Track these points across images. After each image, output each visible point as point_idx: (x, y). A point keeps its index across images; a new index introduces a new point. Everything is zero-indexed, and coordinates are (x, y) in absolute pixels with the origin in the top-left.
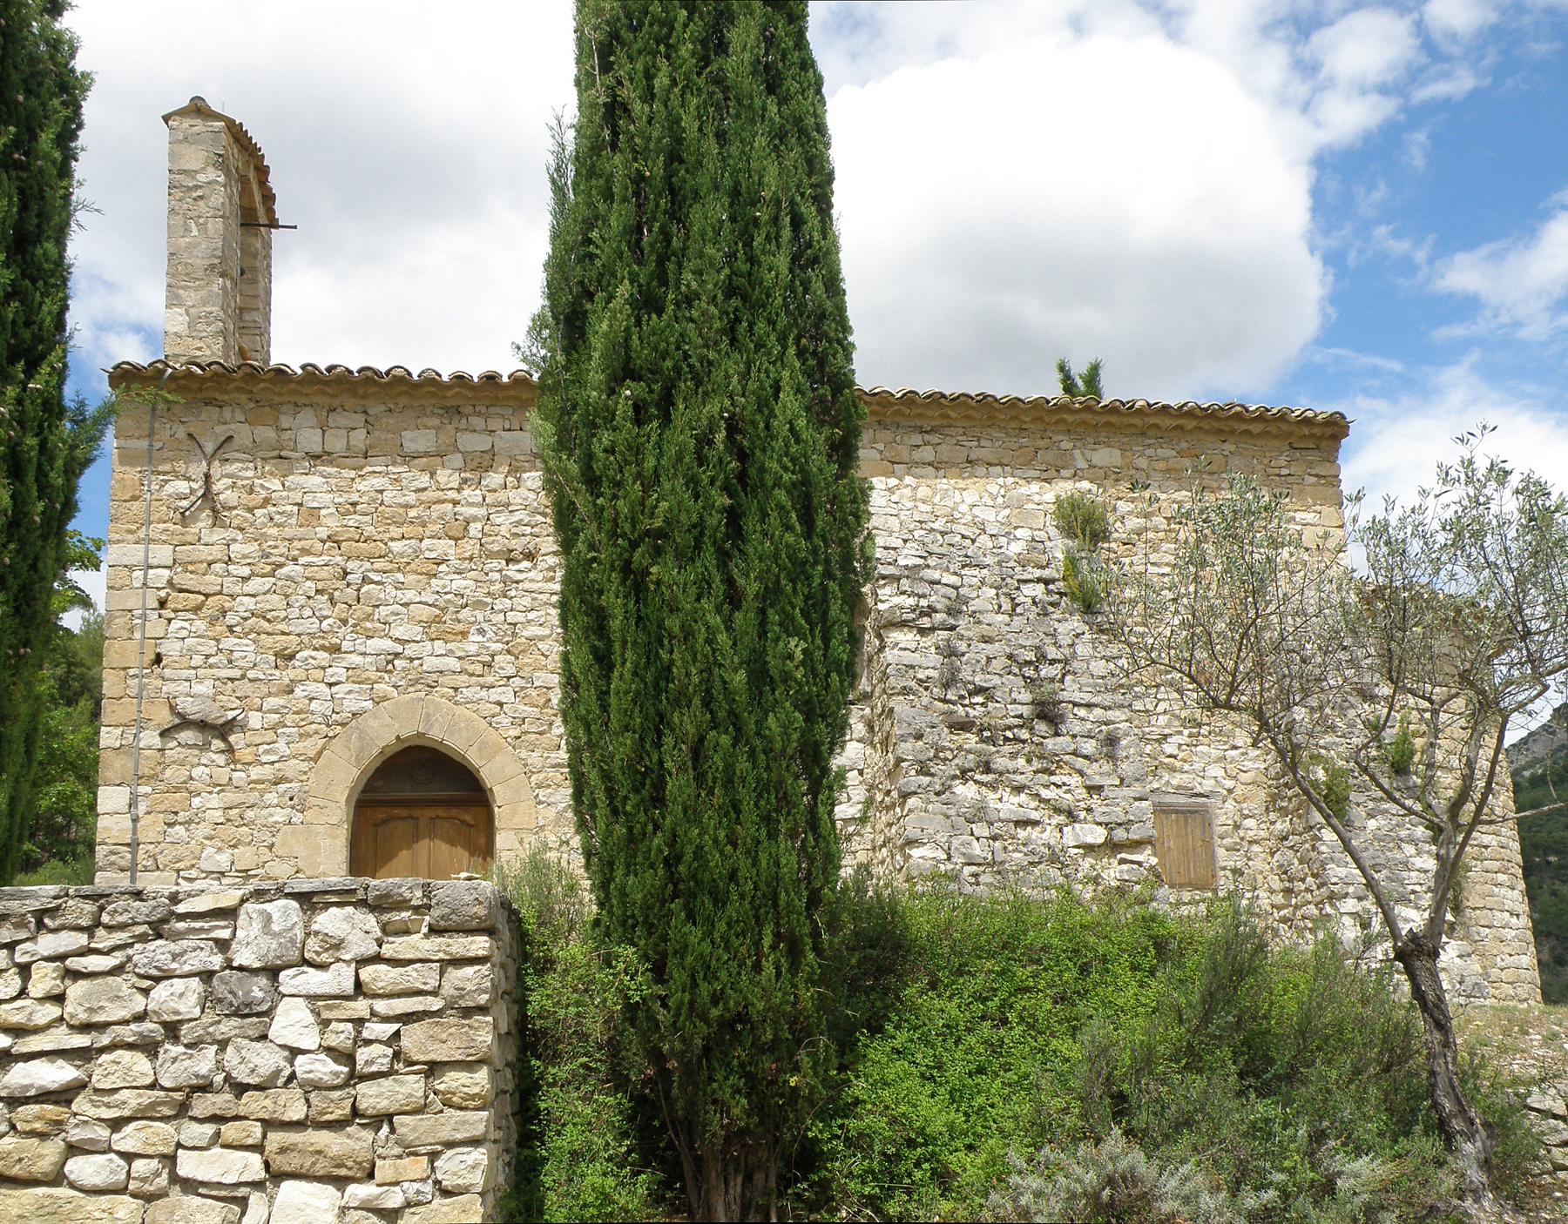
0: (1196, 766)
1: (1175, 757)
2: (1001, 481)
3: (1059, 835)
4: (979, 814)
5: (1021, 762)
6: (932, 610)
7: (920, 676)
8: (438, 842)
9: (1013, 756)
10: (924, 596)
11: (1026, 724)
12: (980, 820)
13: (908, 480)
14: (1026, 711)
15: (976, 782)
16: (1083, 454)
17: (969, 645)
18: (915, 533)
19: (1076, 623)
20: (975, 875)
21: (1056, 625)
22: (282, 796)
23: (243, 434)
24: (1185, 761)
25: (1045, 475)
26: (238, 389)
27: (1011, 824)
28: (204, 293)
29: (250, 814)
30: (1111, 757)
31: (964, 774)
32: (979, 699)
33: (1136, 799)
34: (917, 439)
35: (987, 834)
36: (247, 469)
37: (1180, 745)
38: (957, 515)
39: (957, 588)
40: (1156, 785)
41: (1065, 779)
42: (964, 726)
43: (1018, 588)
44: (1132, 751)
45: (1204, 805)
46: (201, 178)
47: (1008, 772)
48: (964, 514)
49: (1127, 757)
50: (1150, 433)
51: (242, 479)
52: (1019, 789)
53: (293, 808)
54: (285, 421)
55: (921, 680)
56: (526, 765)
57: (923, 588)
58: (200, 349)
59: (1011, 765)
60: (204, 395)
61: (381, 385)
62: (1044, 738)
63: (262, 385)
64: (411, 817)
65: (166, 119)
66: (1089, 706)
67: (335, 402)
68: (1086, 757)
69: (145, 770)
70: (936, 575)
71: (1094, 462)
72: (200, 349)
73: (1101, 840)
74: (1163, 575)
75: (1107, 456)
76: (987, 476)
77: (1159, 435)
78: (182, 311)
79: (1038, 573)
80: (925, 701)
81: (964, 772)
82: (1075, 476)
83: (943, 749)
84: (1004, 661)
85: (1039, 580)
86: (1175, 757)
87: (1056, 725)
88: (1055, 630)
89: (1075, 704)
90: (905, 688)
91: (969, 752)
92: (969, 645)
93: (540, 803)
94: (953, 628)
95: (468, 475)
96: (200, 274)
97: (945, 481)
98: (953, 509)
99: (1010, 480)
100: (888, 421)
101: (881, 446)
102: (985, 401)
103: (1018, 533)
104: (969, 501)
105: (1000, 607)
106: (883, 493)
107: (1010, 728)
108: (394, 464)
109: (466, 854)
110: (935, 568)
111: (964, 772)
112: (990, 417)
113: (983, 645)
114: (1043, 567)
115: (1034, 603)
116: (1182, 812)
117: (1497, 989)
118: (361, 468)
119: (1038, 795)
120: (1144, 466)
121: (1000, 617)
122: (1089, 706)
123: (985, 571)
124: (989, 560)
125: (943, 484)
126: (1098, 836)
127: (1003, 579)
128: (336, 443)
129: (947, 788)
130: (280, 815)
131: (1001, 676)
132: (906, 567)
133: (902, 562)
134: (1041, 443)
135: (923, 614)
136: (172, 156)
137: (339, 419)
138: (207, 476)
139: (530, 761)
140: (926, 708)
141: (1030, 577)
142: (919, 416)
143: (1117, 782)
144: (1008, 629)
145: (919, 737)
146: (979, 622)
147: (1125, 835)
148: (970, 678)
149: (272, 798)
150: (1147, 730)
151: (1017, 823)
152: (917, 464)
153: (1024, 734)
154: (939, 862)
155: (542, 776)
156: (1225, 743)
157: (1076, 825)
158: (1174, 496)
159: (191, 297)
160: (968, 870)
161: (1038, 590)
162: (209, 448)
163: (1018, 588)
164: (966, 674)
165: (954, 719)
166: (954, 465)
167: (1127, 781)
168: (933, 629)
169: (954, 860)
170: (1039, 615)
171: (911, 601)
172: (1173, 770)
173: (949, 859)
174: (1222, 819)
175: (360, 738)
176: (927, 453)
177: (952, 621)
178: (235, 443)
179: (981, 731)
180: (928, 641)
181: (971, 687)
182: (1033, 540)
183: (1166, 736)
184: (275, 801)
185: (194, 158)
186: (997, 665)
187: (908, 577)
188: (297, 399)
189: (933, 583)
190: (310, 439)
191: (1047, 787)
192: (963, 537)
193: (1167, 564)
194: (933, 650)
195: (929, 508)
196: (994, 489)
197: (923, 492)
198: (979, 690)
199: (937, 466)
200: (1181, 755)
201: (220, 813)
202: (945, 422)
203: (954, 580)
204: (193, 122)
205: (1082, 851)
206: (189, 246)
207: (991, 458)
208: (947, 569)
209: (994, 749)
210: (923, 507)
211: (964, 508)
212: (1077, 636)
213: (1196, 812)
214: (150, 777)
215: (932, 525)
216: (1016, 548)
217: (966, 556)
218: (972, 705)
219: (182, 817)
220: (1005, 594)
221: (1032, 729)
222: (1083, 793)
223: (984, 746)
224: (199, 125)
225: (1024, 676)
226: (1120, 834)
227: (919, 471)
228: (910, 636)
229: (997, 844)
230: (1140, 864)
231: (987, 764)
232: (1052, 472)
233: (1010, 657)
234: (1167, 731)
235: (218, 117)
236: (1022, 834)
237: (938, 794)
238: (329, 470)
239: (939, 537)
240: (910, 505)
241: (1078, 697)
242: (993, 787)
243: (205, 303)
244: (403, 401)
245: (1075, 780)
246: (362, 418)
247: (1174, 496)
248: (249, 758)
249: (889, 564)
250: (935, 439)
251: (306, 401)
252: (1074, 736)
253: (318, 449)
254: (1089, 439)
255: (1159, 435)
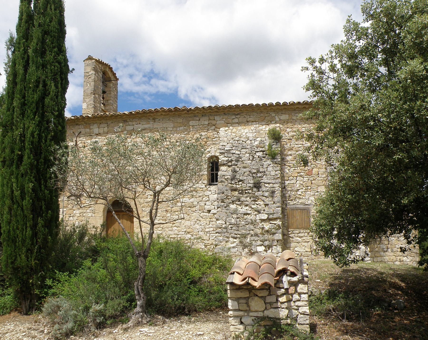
0: (307, 197)
1: (301, 195)
2: (255, 126)
3: (255, 217)
4: (235, 212)
5: (248, 198)
6: (232, 161)
7: (226, 178)
8: (124, 220)
9: (246, 197)
10: (230, 157)
11: (251, 189)
12: (235, 214)
13: (231, 128)
14: (251, 185)
15: (236, 204)
16: (278, 117)
17: (240, 169)
18: (230, 141)
19: (269, 162)
20: (232, 227)
21: (264, 162)
22: (90, 210)
23: (83, 131)
24: (303, 196)
25: (267, 123)
26: (82, 121)
27: (243, 215)
28: (90, 99)
29: (84, 214)
30: (272, 197)
31: (233, 202)
32: (241, 183)
33: (277, 207)
34: (234, 117)
35: (236, 217)
36: (84, 139)
37: (302, 192)
38: (242, 136)
39: (239, 155)
40: (295, 203)
41: (259, 202)
42: (235, 190)
43: (255, 154)
44: (278, 195)
45: (308, 207)
46: (90, 73)
47: (244, 201)
48: (244, 135)
49: (276, 196)
50: (297, 110)
51: (83, 141)
52: (246, 205)
54: (91, 127)
55: (226, 179)
56: (140, 202)
57: (231, 155)
58: (89, 111)
59: (245, 199)
60: (76, 123)
61: (109, 117)
62: (255, 192)
63: (86, 120)
65: (84, 61)
66: (269, 183)
67: (101, 122)
68: (266, 197)
69: (65, 205)
70: (234, 152)
71: (281, 119)
72: (89, 111)
73: (266, 218)
74: (299, 147)
75: (284, 117)
76: (252, 125)
77: (300, 110)
78: (86, 103)
79: (261, 149)
80: (226, 184)
81: (233, 202)
82: (276, 123)
83: (229, 196)
84: (248, 173)
85: (261, 151)
86: (301, 195)
87: (258, 189)
88: (263, 164)
89: (265, 183)
90: (221, 181)
91: (235, 196)
92: (240, 169)
93: (143, 211)
94: (236, 165)
95: (128, 136)
96: (89, 95)
97: (240, 127)
98: (241, 134)
99: (258, 125)
100: (226, 113)
101: (224, 120)
102: (251, 106)
103: (257, 139)
104: (245, 132)
105: (249, 159)
106: (224, 132)
107: (247, 190)
108: (113, 135)
110: (234, 150)
111: (233, 202)
112: (253, 110)
113: (243, 169)
114: (263, 148)
115: (259, 157)
116: (302, 209)
117: (395, 253)
118: (106, 136)
119: (251, 207)
120: (295, 119)
121: (249, 162)
122: (269, 183)
123: (247, 150)
124: (248, 147)
125: (240, 128)
126: (265, 217)
127: (251, 152)
128: (101, 131)
129: (228, 206)
130: (90, 215)
131: (247, 177)
132: (226, 150)
133: (226, 149)
134: (267, 115)
135: (229, 162)
136: (85, 69)
137: (102, 125)
138: (76, 141)
139: (141, 201)
140: (226, 186)
141: (259, 150)
142: (235, 111)
143: (273, 203)
144: (251, 164)
145: (223, 193)
146: (244, 163)
147: (272, 217)
148: (238, 178)
149: (88, 211)
150: (293, 188)
151: (244, 214)
152: (234, 123)
153: (250, 191)
154: (223, 224)
155: (143, 205)
156: (315, 191)
157: (260, 214)
158: (303, 126)
159: (87, 100)
160: (230, 226)
161: (260, 154)
162: (77, 135)
163: (255, 154)
164: (237, 177)
165: (233, 188)
166: (243, 123)
167: (275, 203)
168: (231, 166)
169: (227, 224)
170: (259, 160)
171: (227, 159)
172: (300, 198)
173: (226, 223)
174: (313, 211)
176: (236, 120)
177: (236, 163)
178: (82, 133)
179: (239, 191)
180: (230, 168)
181: (238, 180)
182: (261, 140)
183: (298, 190)
185: (89, 69)
186: (246, 174)
187: (226, 153)
188: (93, 122)
189: (233, 154)
190: (96, 131)
191: (254, 205)
192: (243, 141)
193: (300, 144)
194: (231, 171)
195: (235, 135)
196: (252, 128)
197: (234, 130)
198: (241, 181)
199: (239, 123)
200: (302, 194)
201: (79, 214)
202: (241, 112)
203: (239, 152)
204: (89, 61)
205: (260, 221)
206: (87, 89)
207: (253, 120)
208: (237, 150)
209: (242, 195)
210: (234, 134)
211: (244, 134)
212: (269, 165)
213: (306, 209)
214: (66, 207)
215: (235, 139)
216: (257, 143)
217: (243, 146)
218: (239, 185)
219: (72, 215)
220: (251, 155)
221: (252, 190)
222: (264, 206)
223: (239, 195)
224: (90, 62)
225: (253, 177)
226: (271, 216)
227: (234, 125)
228: (226, 168)
229: (238, 220)
230: (275, 224)
231: (239, 199)
232: (269, 122)
233: (250, 172)
234: (299, 188)
235: (94, 59)
236: (245, 217)
237: (225, 207)
238: (100, 137)
239: (236, 142)
240: (230, 134)
241: (266, 181)
242: (240, 205)
243: (90, 101)
244: (115, 120)
245: (262, 203)
246: (106, 125)
247: (303, 126)
248: (84, 202)
249: (223, 149)
250: (238, 116)
251: (95, 122)
252: (263, 191)
253: (97, 133)
254: (280, 113)
255: (300, 110)
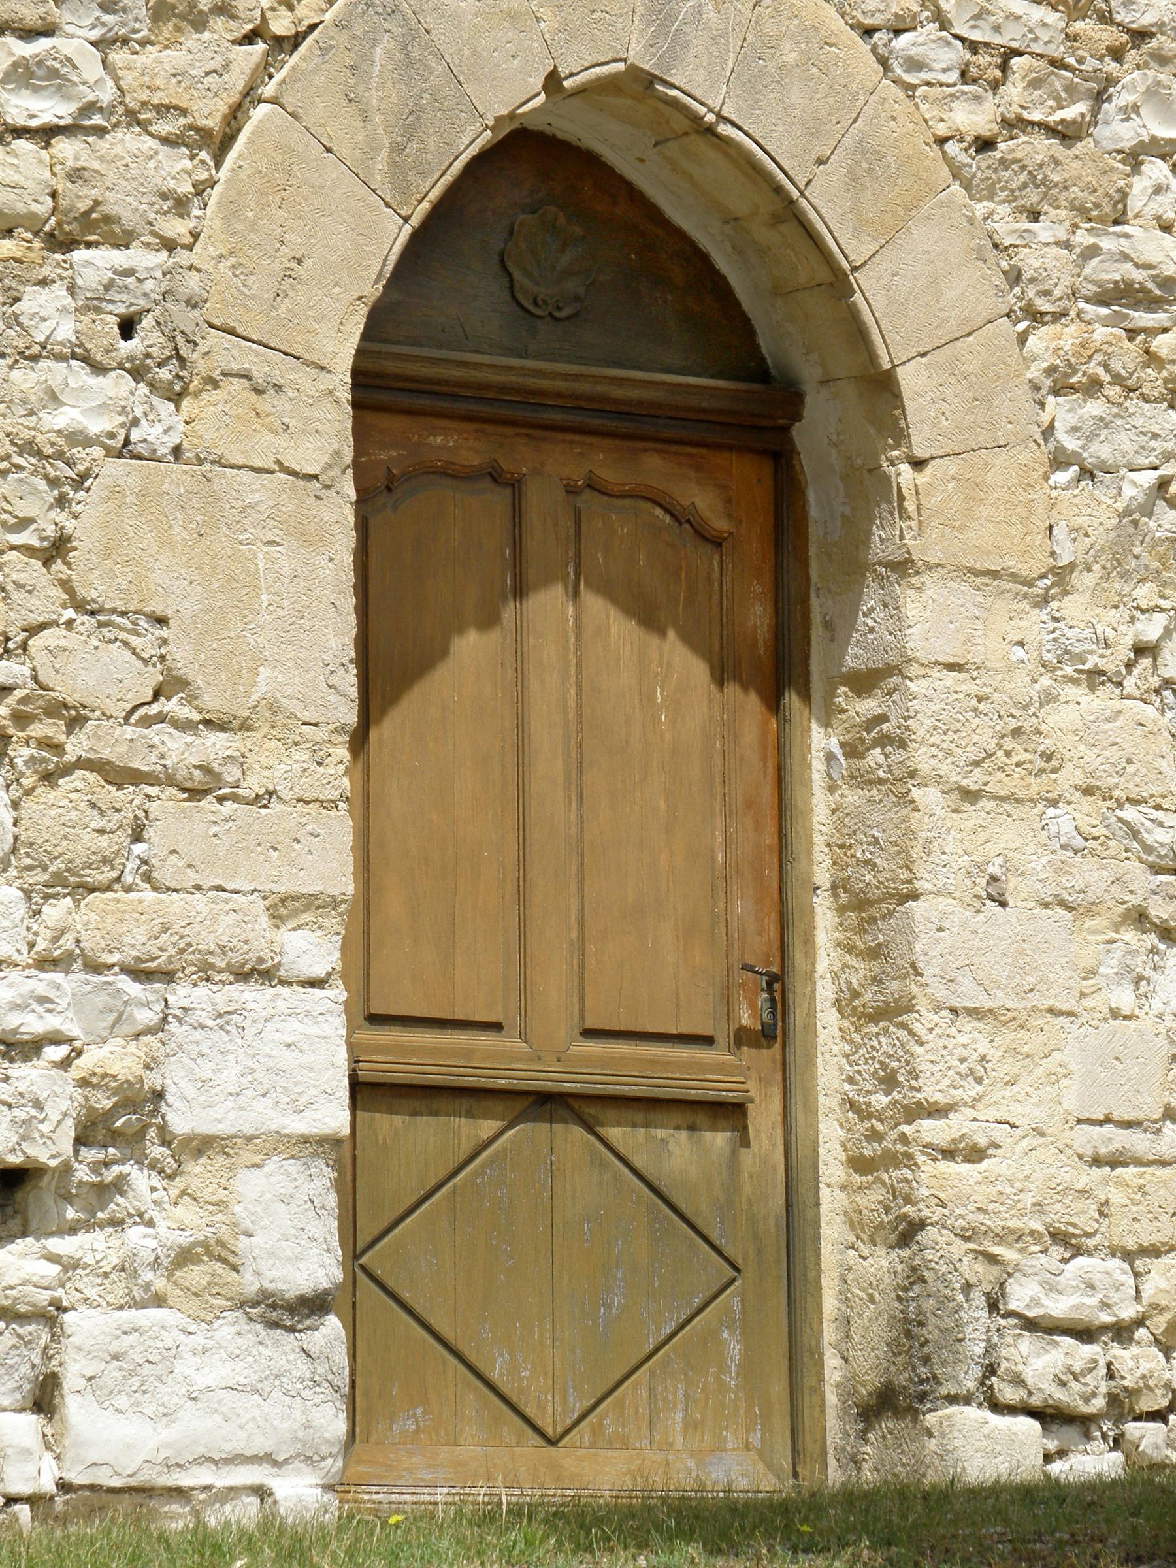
8: (593, 603)
53: (137, 373)
56: (1015, 277)
64: (495, 476)
93: (1060, 460)
109: (699, 670)
139: (1029, 261)
155: (1068, 335)
175: (408, 65)
184: (65, 331)
